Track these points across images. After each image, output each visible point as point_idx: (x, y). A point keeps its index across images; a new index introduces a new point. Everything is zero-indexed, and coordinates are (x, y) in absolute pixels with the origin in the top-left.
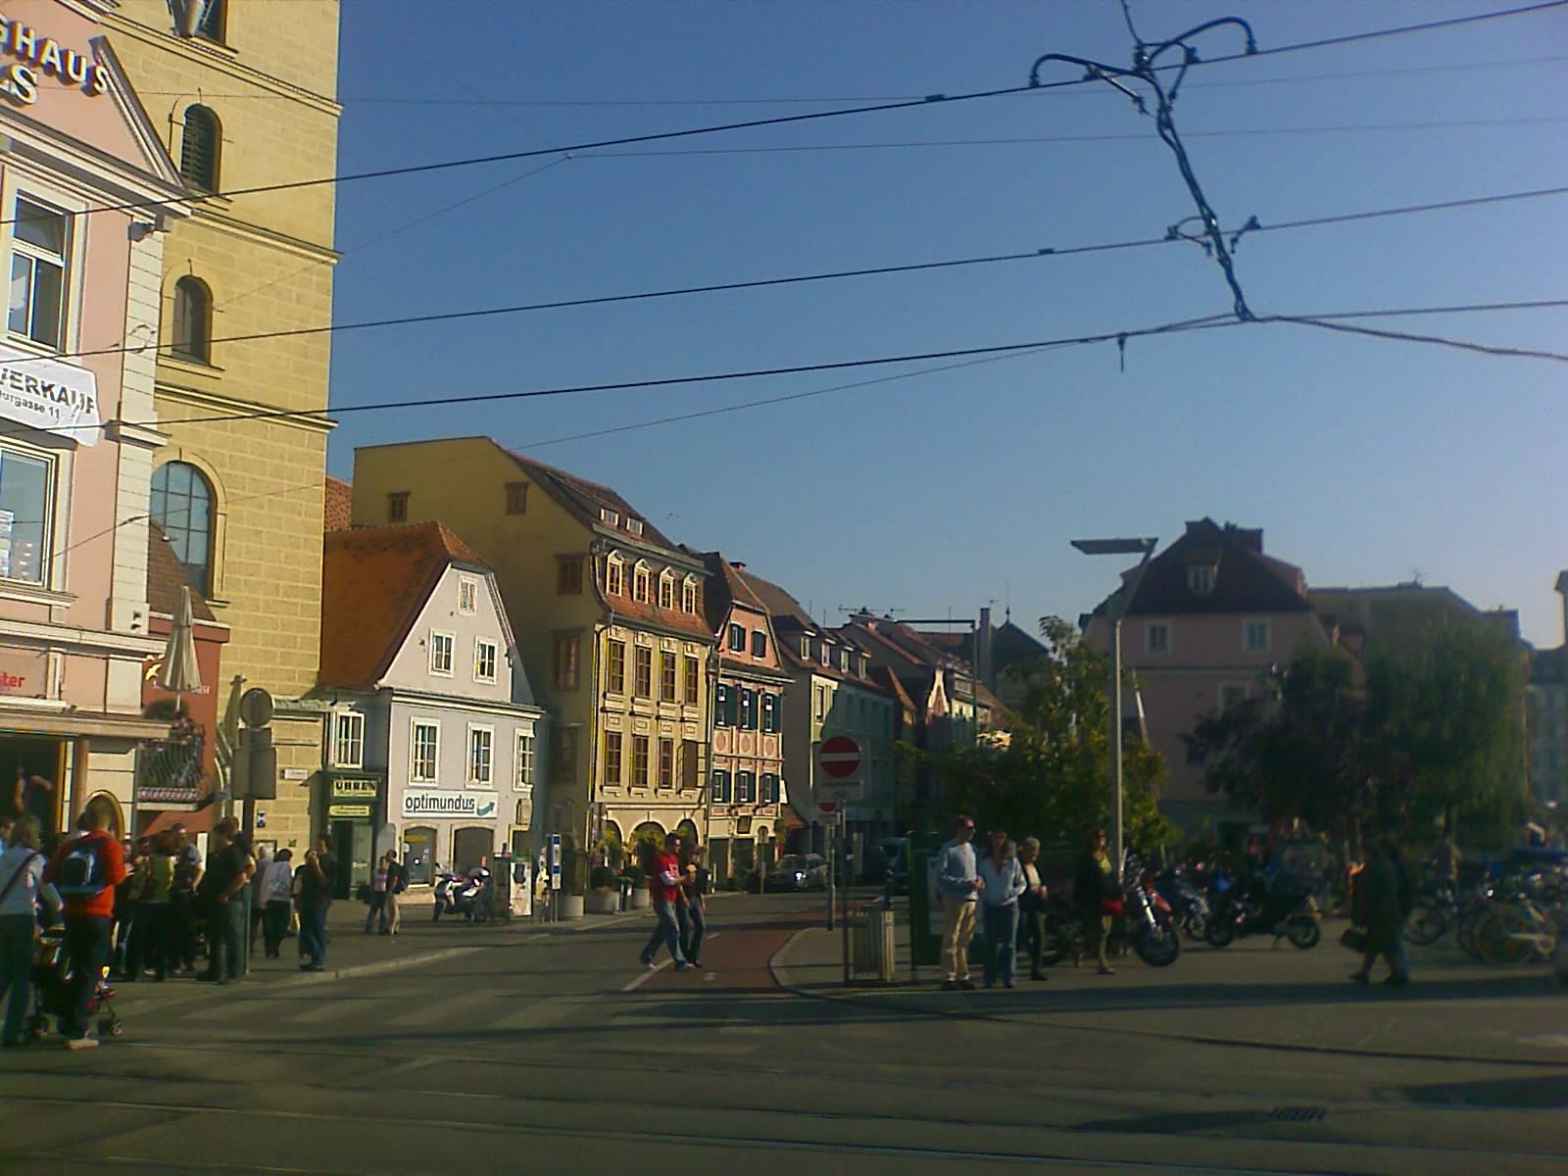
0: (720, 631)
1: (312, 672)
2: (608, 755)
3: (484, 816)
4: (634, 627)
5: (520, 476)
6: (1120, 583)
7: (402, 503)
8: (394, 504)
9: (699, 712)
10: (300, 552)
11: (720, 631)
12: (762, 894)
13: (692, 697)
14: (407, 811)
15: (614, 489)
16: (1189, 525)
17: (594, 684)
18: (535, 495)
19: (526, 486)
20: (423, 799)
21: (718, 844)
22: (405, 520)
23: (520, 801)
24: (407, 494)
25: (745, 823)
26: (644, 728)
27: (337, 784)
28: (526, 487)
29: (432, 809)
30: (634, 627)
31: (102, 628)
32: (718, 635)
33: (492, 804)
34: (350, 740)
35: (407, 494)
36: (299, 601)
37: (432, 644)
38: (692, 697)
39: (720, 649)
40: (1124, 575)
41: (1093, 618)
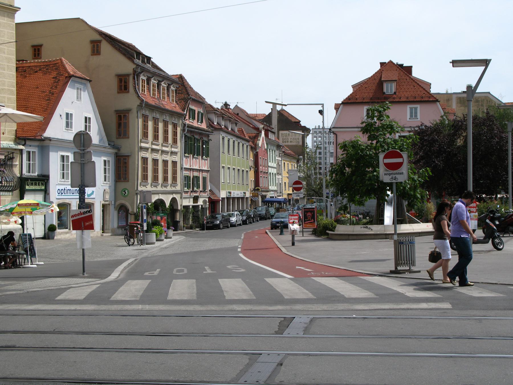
0: (186, 111)
1: (14, 130)
2: (164, 177)
3: (90, 197)
4: (153, 108)
5: (98, 38)
6: (350, 91)
7: (39, 50)
8: (35, 50)
9: (179, 148)
10: (6, 72)
11: (186, 111)
12: (205, 230)
13: (175, 141)
14: (58, 196)
15: (134, 44)
16: (382, 64)
17: (136, 135)
18: (105, 47)
19: (100, 42)
20: (65, 190)
21: (186, 207)
22: (41, 58)
23: (105, 190)
24: (41, 46)
25: (196, 199)
26: (170, 159)
27: (27, 183)
28: (101, 42)
29: (68, 194)
30: (153, 108)
31: (302, 236)
32: (185, 113)
33: (93, 192)
34: (31, 162)
35: (41, 46)
36: (6, 96)
37: (64, 117)
38: (175, 141)
39: (186, 119)
40: (354, 87)
41: (341, 106)
